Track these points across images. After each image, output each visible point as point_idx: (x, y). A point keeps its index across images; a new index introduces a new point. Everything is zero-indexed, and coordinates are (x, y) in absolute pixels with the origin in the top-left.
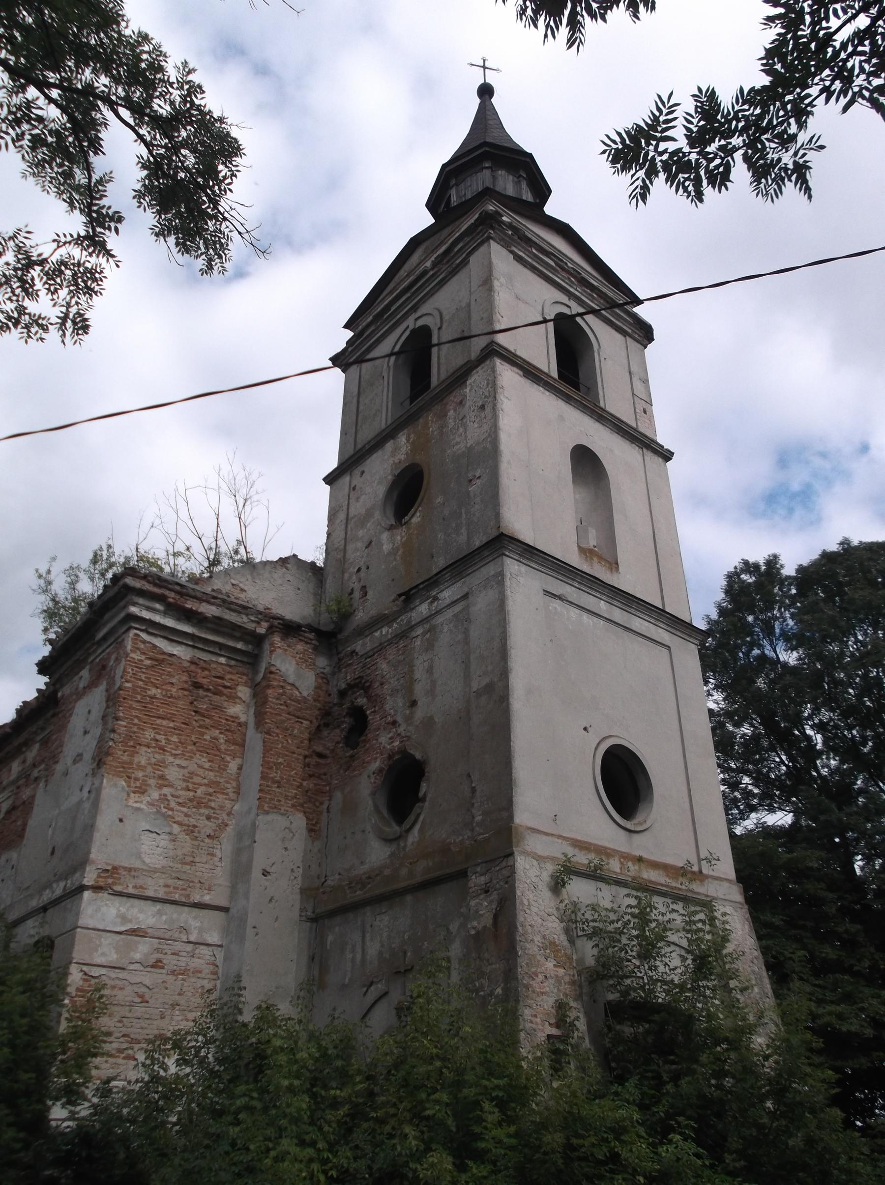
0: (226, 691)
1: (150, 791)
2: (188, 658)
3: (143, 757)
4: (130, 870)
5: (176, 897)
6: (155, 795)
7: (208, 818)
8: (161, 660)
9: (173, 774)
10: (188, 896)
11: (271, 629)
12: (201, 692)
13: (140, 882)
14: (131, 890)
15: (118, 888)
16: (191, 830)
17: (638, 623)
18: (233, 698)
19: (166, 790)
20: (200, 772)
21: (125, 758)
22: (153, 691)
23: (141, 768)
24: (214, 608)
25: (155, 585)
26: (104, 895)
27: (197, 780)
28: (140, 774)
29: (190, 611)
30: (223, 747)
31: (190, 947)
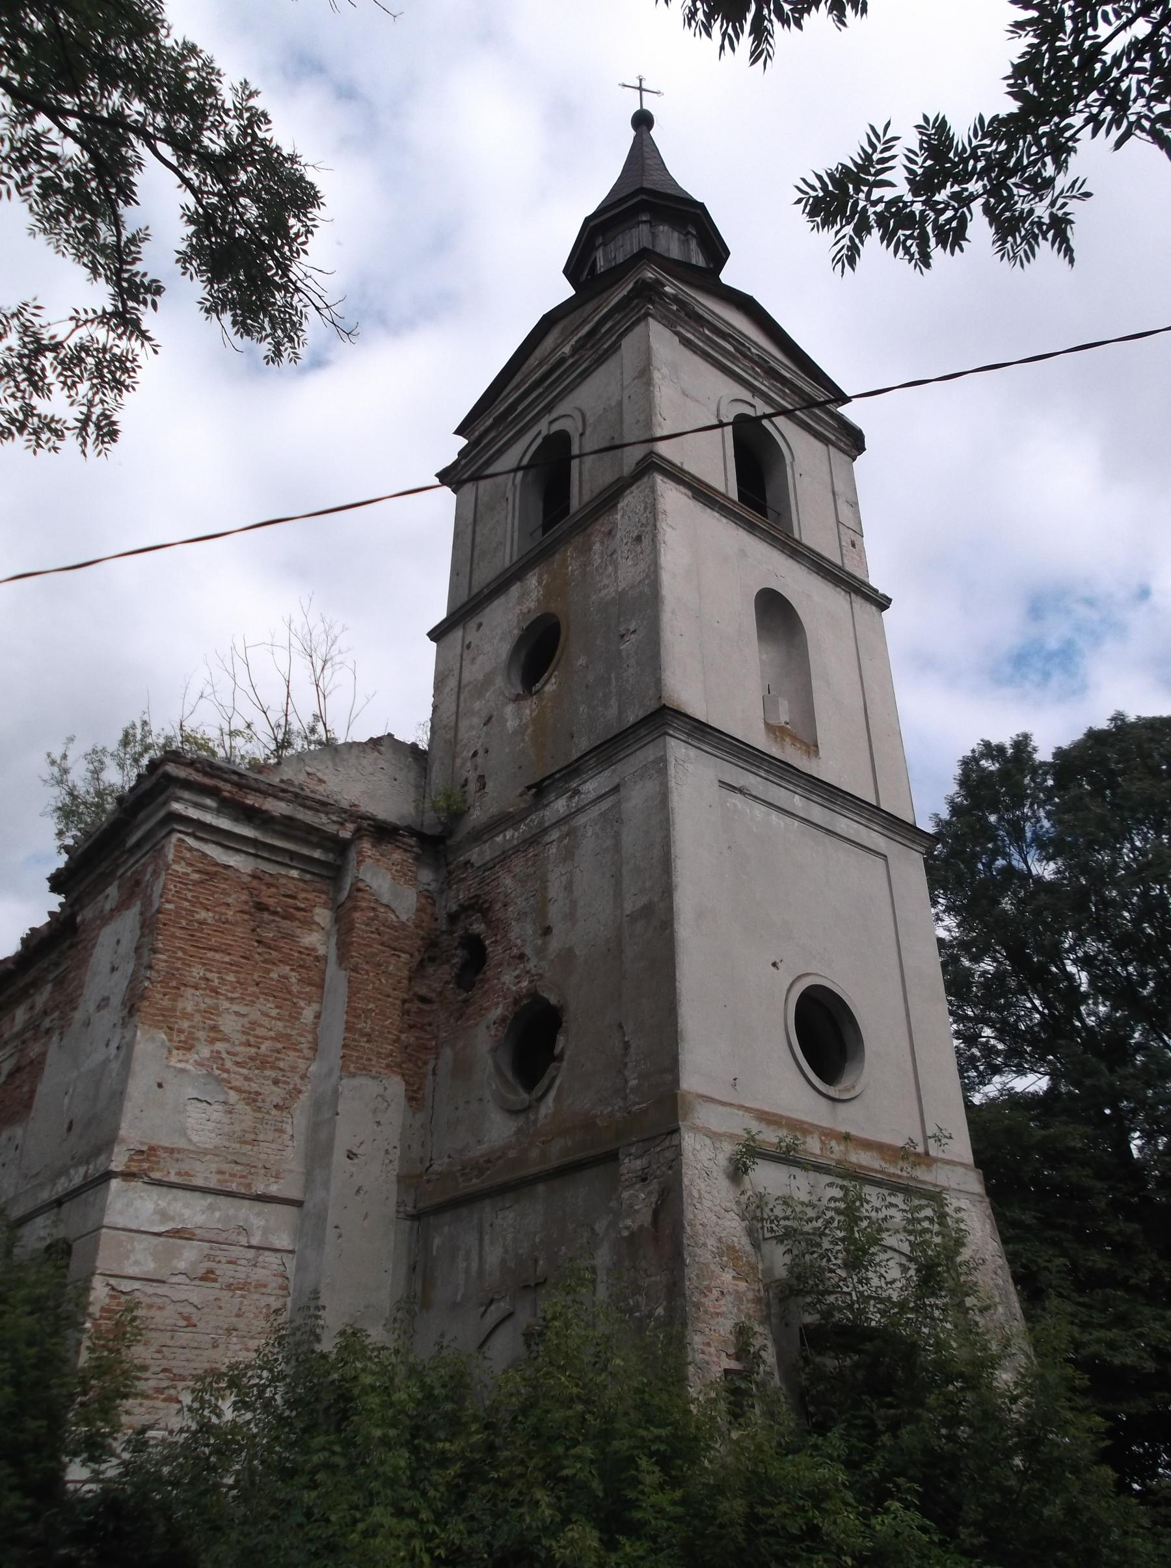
0: (299, 914)
1: (199, 1047)
2: (249, 871)
3: (189, 1001)
4: (172, 1151)
5: (233, 1187)
6: (205, 1052)
7: (276, 1082)
8: (213, 873)
9: (229, 1024)
10: (249, 1186)
11: (358, 833)
12: (266, 916)
13: (185, 1167)
14: (173, 1178)
15: (156, 1175)
16: (252, 1099)
17: (845, 825)
18: (309, 924)
19: (219, 1046)
20: (265, 1021)
21: (166, 1003)
22: (203, 915)
23: (187, 1016)
24: (283, 804)
25: (205, 774)
26: (138, 1184)
27: (261, 1032)
28: (185, 1024)
29: (252, 808)
30: (295, 989)
31: (251, 1254)
